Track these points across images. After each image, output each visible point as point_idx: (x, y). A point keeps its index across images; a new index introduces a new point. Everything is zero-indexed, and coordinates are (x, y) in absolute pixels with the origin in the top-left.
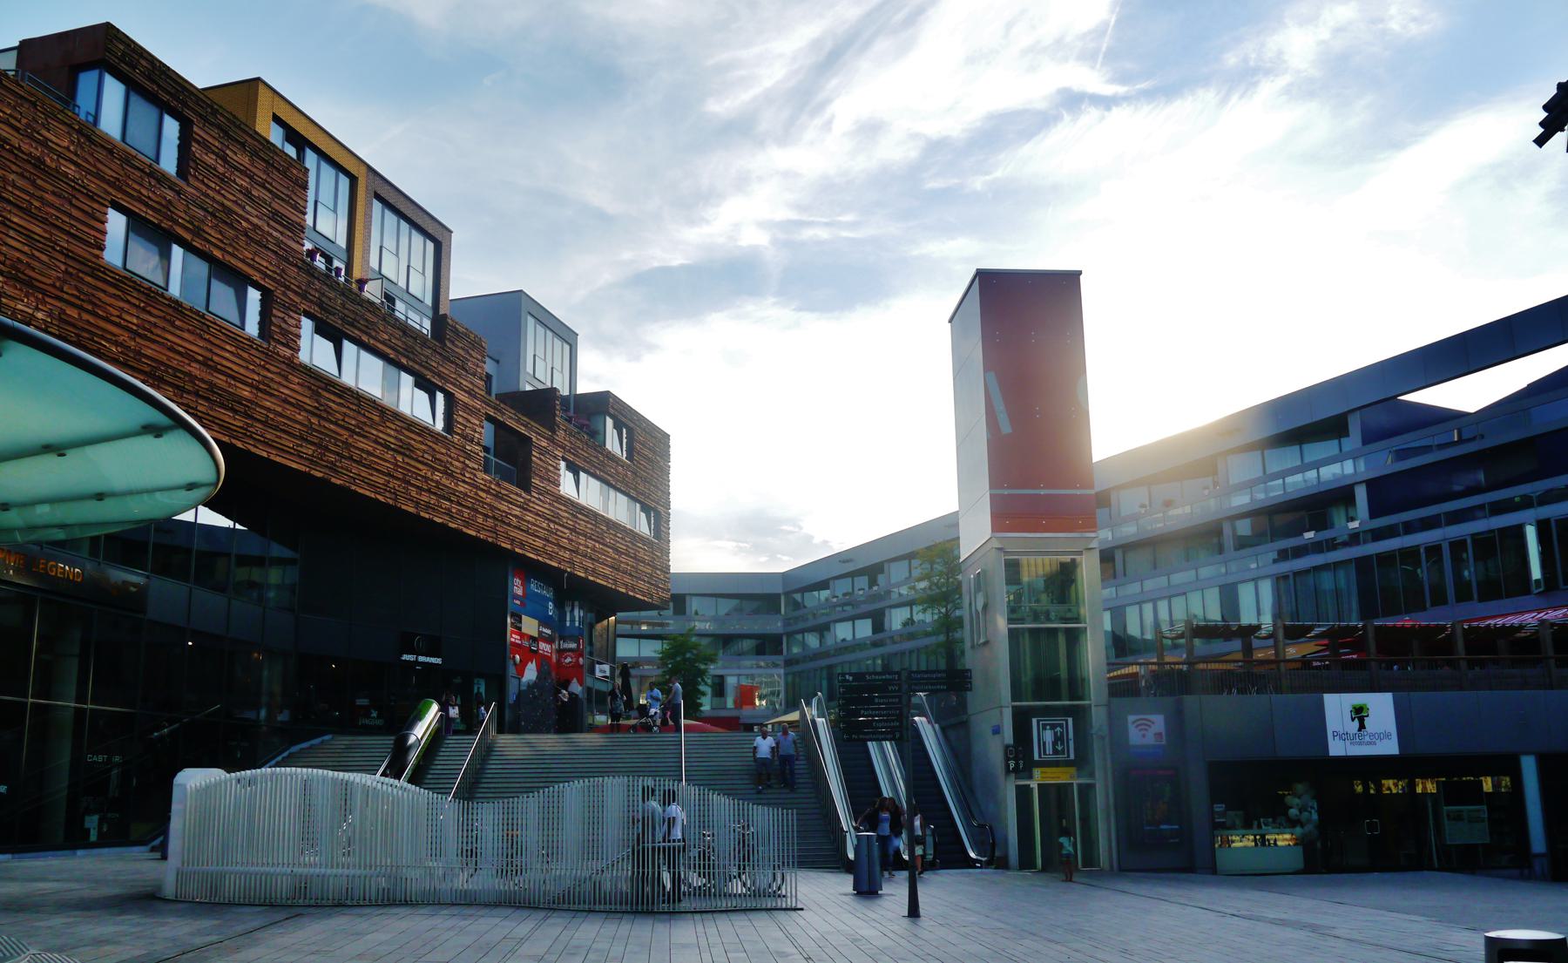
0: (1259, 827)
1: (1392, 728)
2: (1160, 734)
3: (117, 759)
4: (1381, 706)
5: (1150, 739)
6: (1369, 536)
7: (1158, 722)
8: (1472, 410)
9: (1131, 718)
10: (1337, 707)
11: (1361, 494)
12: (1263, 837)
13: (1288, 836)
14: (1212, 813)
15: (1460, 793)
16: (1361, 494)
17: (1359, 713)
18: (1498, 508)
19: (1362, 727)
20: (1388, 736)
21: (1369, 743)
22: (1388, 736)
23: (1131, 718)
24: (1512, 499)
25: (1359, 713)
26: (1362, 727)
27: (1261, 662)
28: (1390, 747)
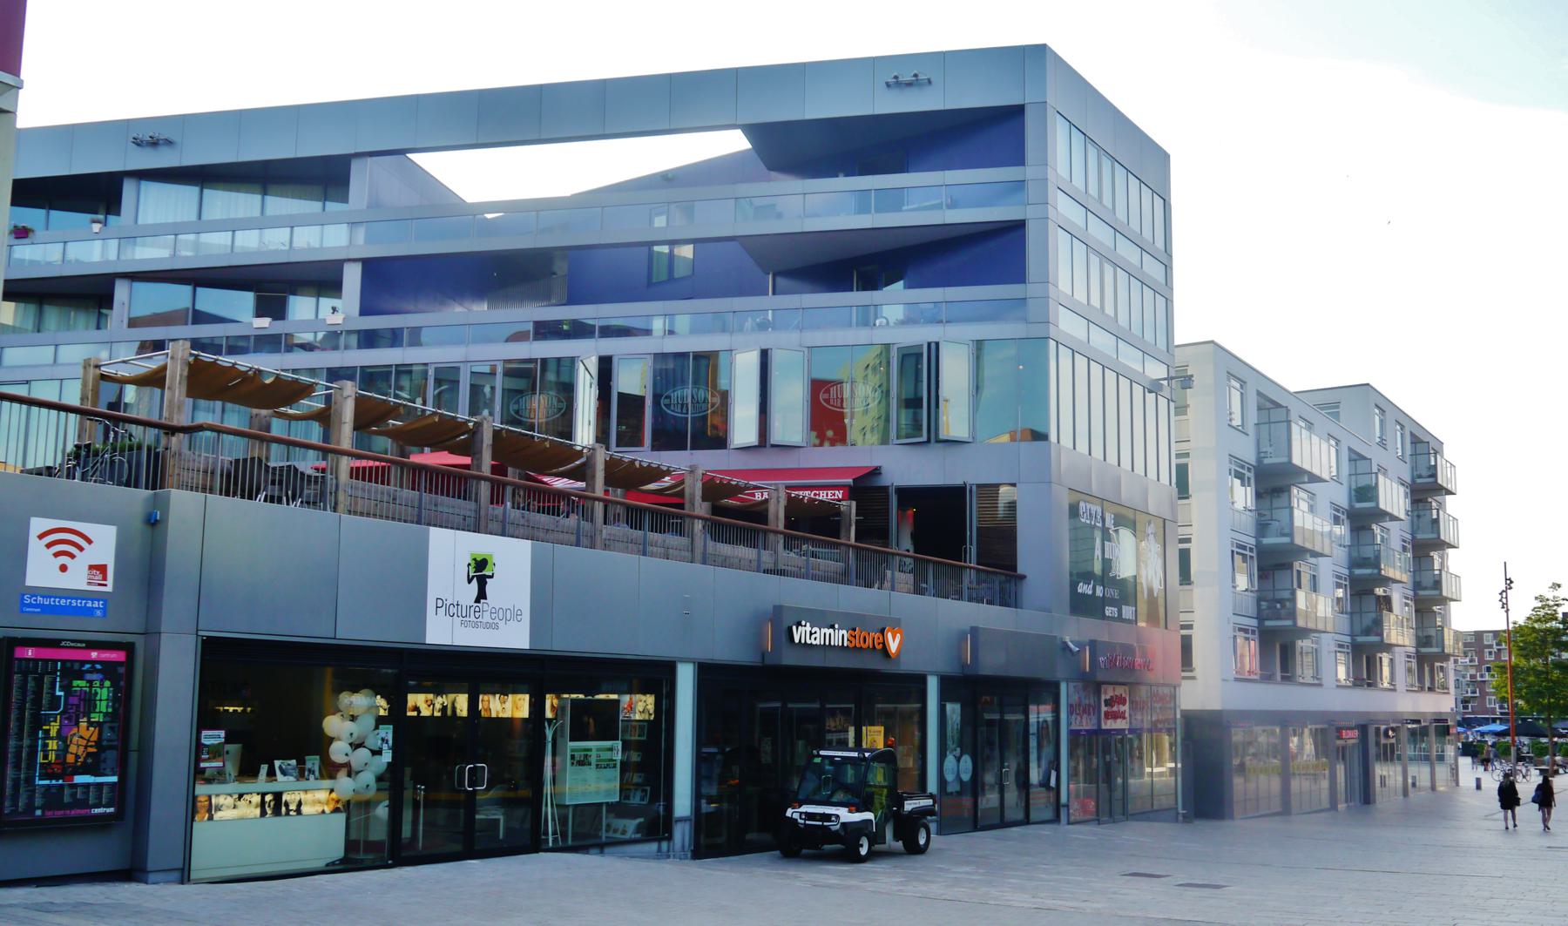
0: (271, 774)
1: (525, 605)
2: (102, 569)
3: (39, 812)
4: (513, 558)
5: (77, 578)
6: (354, 340)
7: (103, 543)
8: (469, 200)
9: (38, 525)
10: (449, 550)
11: (352, 278)
12: (278, 796)
13: (323, 795)
14: (199, 746)
15: (595, 722)
16: (352, 278)
17: (480, 571)
18: (546, 330)
19: (482, 595)
20: (517, 615)
21: (488, 626)
22: (517, 615)
23: (38, 525)
24: (560, 322)
25: (480, 571)
26: (482, 595)
27: (661, 214)
28: (515, 637)
